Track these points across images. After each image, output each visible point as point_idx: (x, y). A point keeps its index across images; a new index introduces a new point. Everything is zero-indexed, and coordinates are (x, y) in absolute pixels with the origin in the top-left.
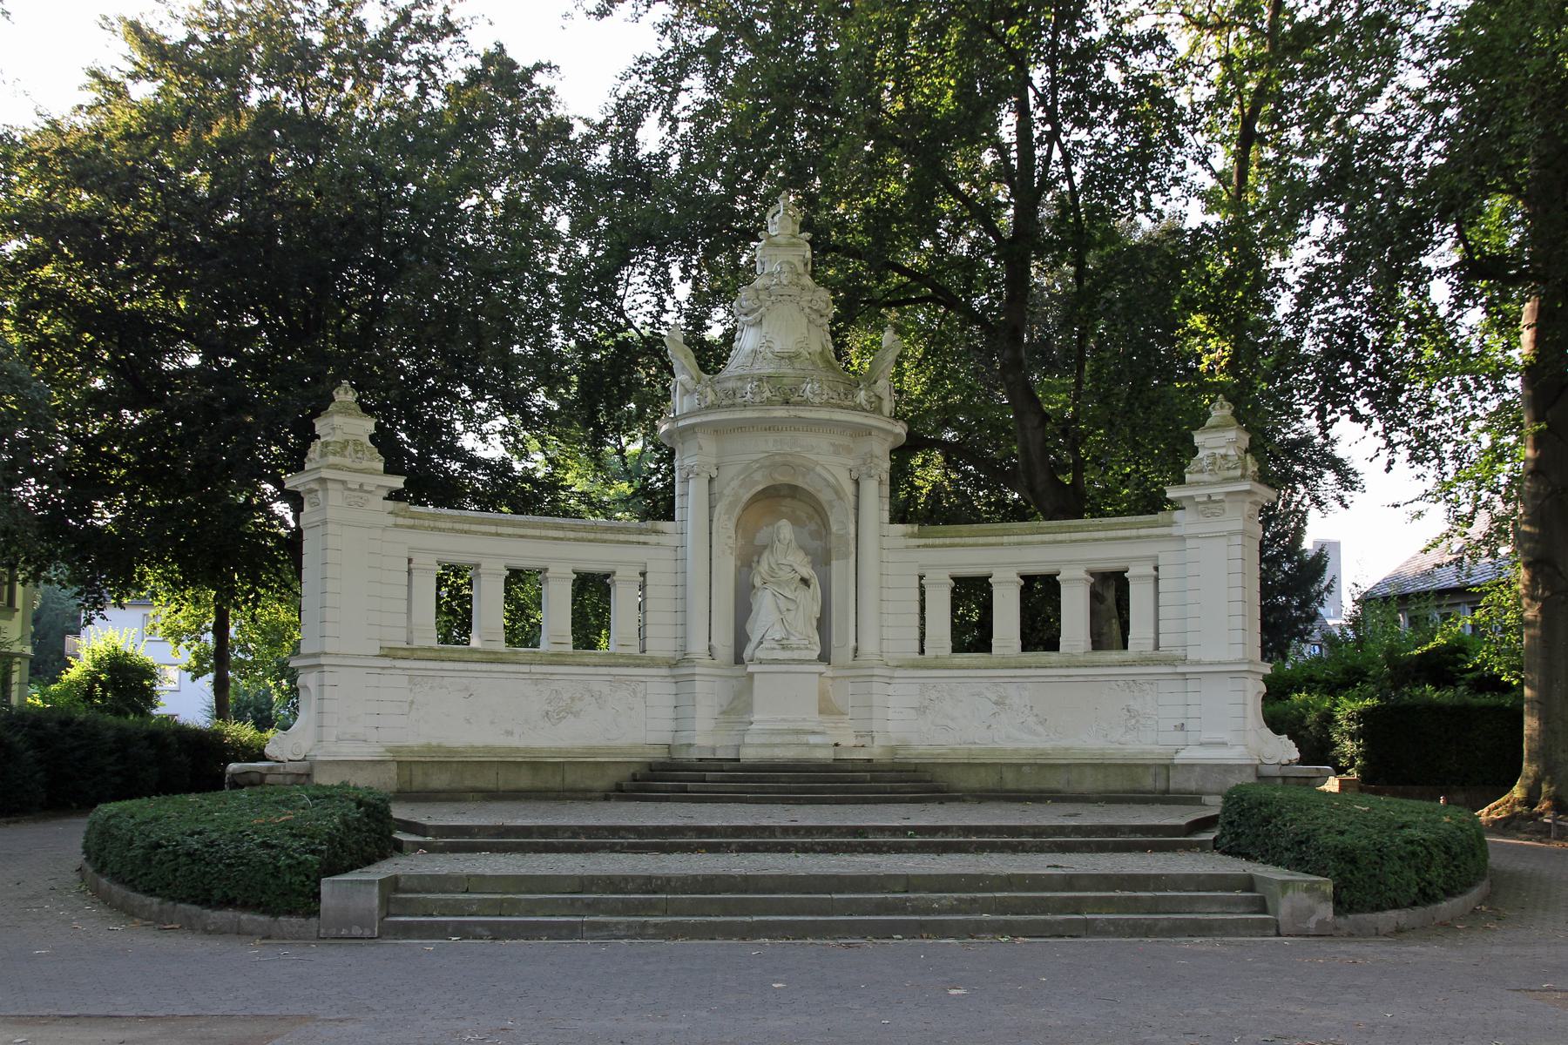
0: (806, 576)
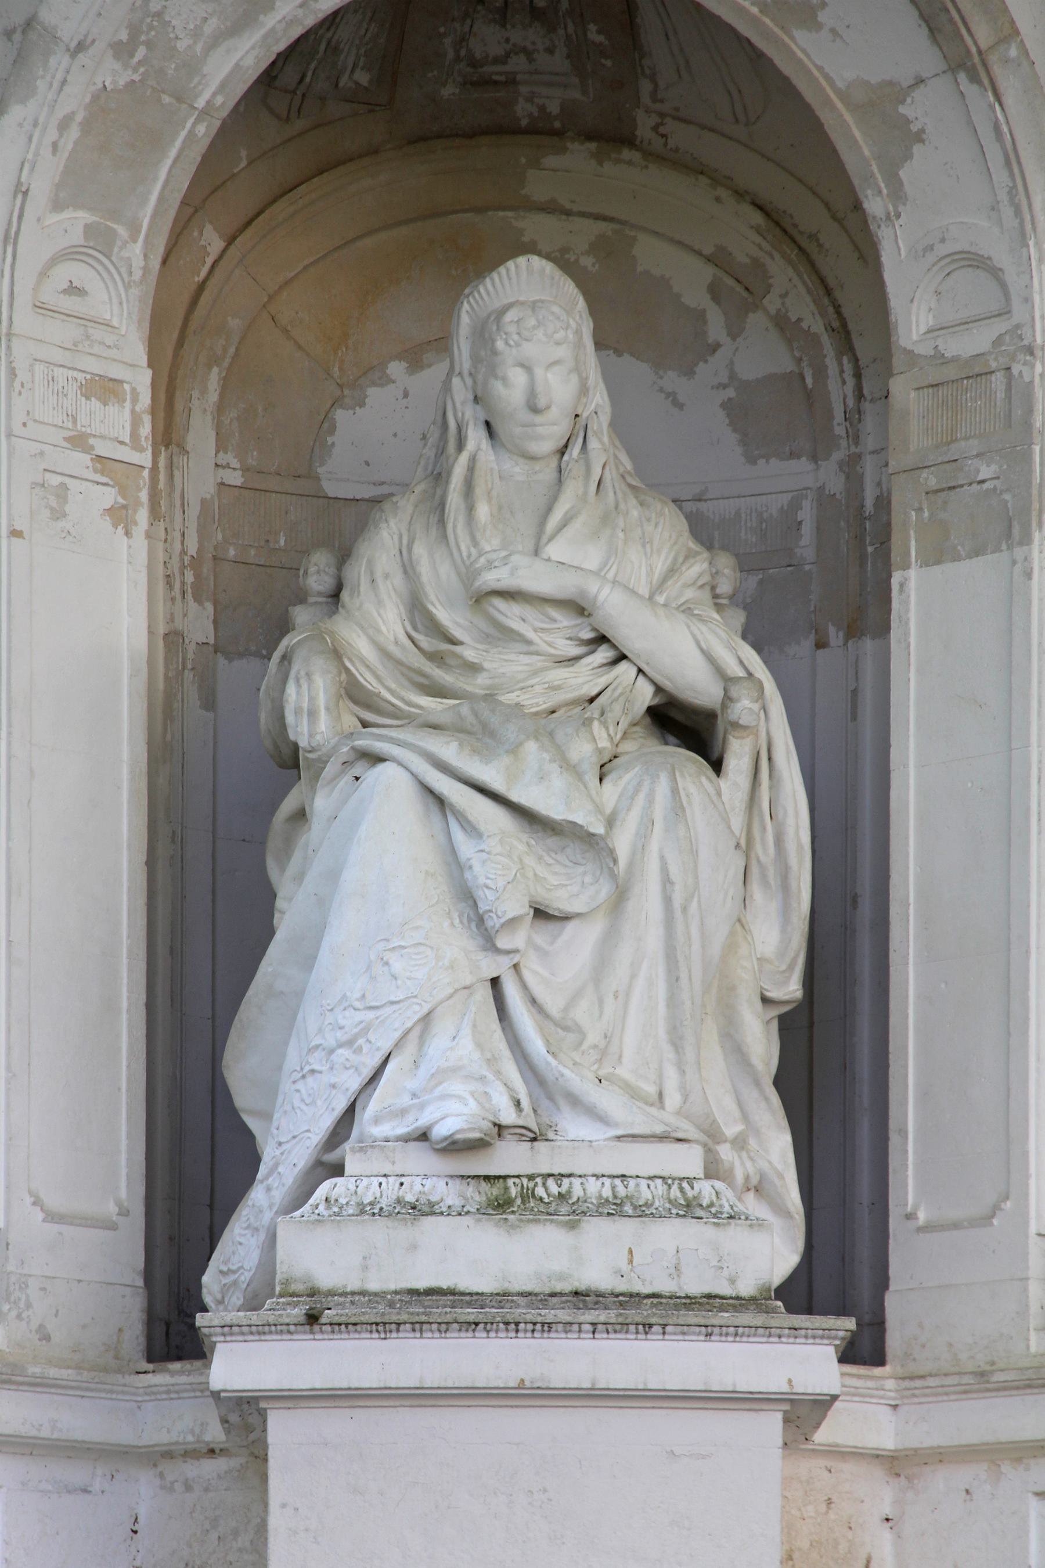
0: (698, 686)
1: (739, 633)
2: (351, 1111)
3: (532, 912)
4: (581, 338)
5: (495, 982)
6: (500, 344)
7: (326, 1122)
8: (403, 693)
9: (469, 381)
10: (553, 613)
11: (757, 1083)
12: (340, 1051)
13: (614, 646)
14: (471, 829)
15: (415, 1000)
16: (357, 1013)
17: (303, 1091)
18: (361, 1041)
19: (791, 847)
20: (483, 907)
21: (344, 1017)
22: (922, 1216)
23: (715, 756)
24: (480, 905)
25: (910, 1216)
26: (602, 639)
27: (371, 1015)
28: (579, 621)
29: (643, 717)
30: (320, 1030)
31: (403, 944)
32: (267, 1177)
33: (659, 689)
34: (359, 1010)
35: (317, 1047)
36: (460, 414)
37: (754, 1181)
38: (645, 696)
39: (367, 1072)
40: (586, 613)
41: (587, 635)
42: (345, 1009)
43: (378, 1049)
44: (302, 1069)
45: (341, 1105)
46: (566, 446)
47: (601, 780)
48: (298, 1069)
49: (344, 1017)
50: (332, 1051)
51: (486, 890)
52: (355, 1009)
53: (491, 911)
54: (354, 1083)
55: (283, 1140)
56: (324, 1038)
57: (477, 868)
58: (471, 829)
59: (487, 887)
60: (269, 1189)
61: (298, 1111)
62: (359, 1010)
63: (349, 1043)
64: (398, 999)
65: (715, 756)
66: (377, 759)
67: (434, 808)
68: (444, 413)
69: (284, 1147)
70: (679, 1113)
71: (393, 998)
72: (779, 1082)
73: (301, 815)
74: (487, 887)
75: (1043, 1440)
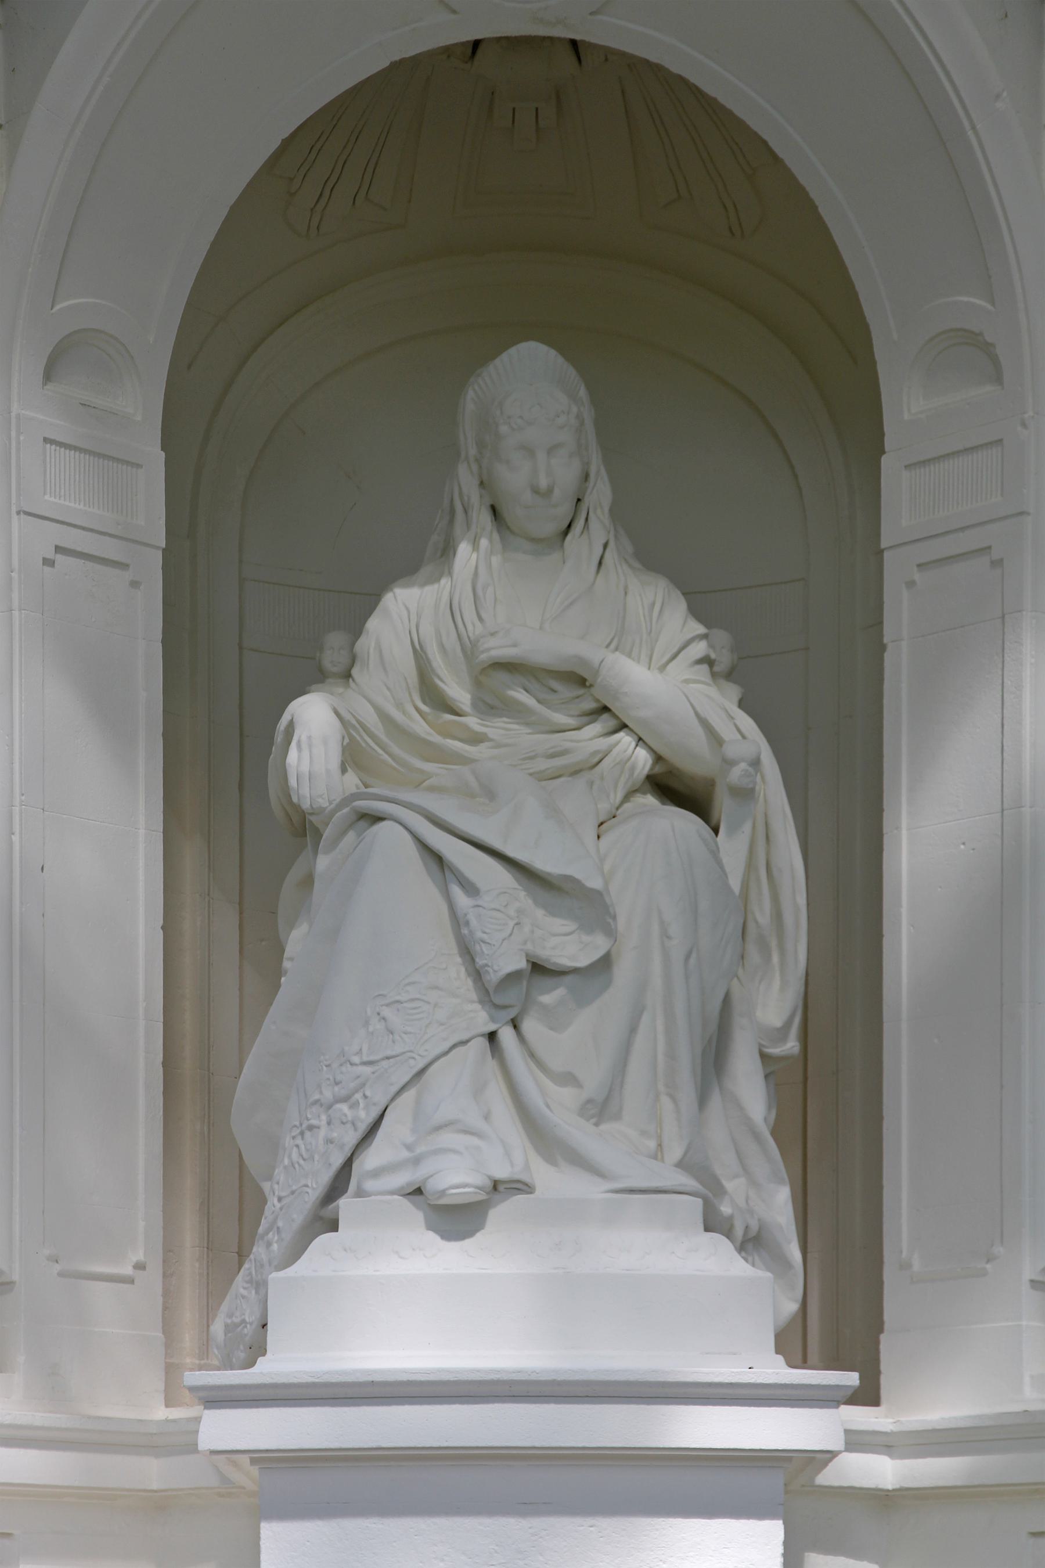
0: (695, 759)
1: (736, 703)
2: (348, 1164)
3: (530, 965)
4: (582, 424)
5: (492, 1036)
6: (504, 429)
7: (325, 1177)
8: (396, 750)
9: (475, 467)
10: (554, 684)
11: (757, 1137)
12: (338, 1106)
13: (615, 716)
14: (471, 889)
15: (409, 1054)
16: (355, 1067)
17: (302, 1147)
18: (358, 1096)
19: (788, 919)
20: (480, 962)
21: (342, 1073)
22: (917, 1266)
23: (714, 822)
24: (477, 960)
25: (905, 1266)
26: (605, 709)
27: (367, 1070)
28: (582, 691)
29: (644, 782)
30: (319, 1086)
31: (398, 998)
32: (267, 1232)
33: (658, 758)
34: (356, 1065)
35: (316, 1102)
36: (466, 498)
37: (754, 1231)
38: (643, 759)
39: (363, 1127)
40: (587, 684)
41: (589, 705)
42: (341, 1065)
43: (374, 1104)
44: (301, 1125)
45: (337, 1160)
46: (569, 526)
47: (599, 837)
48: (297, 1123)
49: (342, 1073)
50: (330, 1107)
51: (483, 945)
52: (351, 1064)
53: (487, 965)
54: (351, 1138)
55: (283, 1194)
56: (321, 1093)
57: (474, 922)
58: (471, 889)
59: (484, 942)
60: (269, 1244)
61: (297, 1166)
62: (356, 1065)
63: (345, 1099)
64: (394, 1053)
65: (714, 822)
66: (377, 819)
67: (434, 867)
68: (452, 500)
69: (284, 1202)
70: (680, 1165)
71: (389, 1053)
72: (776, 1132)
73: (308, 881)
74: (484, 942)
75: (1043, 1484)
